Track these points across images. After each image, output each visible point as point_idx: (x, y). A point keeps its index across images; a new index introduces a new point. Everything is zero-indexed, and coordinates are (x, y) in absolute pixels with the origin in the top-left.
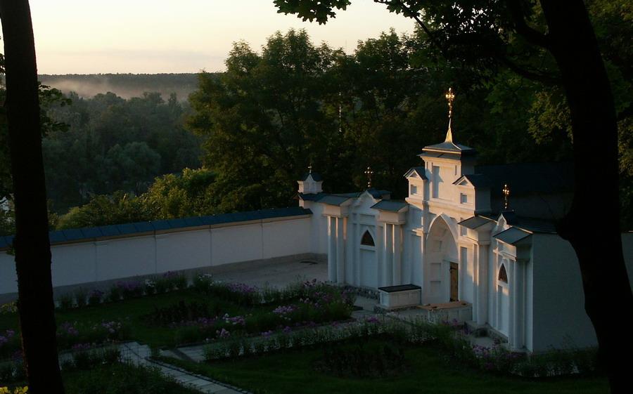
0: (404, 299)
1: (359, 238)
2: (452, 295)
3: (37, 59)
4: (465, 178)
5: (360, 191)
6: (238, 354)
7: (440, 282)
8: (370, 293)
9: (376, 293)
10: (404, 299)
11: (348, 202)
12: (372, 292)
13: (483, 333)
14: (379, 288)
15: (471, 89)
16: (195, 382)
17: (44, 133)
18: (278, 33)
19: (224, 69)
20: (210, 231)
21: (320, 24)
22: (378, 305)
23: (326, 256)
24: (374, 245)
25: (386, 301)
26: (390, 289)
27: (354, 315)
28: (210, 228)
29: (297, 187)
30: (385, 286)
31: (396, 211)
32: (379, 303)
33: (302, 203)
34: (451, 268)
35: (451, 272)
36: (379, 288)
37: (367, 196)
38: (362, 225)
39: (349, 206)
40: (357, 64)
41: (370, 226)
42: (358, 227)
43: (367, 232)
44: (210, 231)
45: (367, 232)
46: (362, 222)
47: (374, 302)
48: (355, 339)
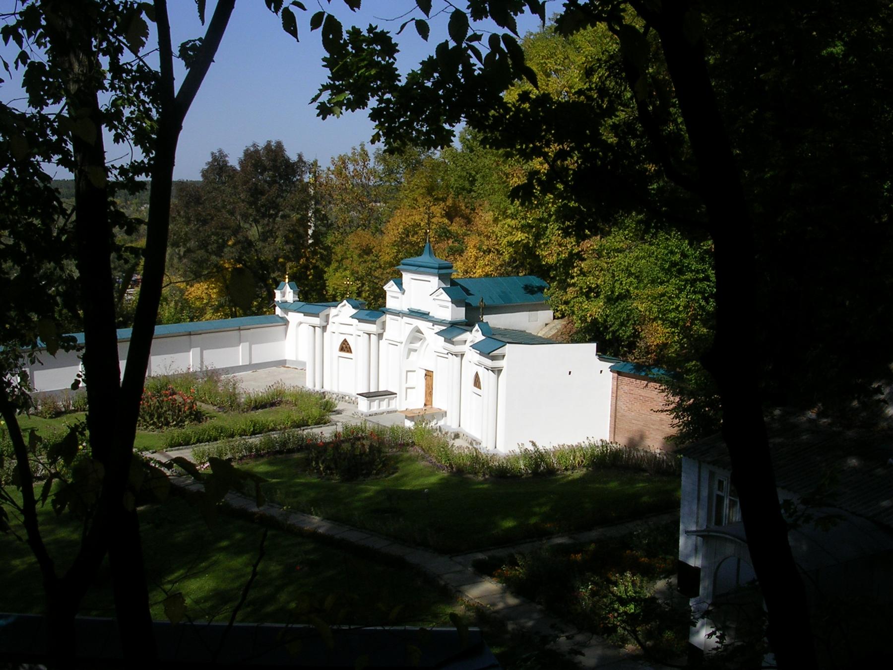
2: (426, 400)
3: (188, 112)
4: (441, 290)
8: (347, 398)
12: (349, 398)
13: (457, 436)
15: (397, 83)
18: (254, 145)
19: (198, 178)
21: (398, 51)
23: (304, 364)
25: (363, 405)
26: (369, 395)
27: (334, 417)
29: (274, 295)
33: (278, 311)
34: (426, 375)
35: (426, 379)
37: (345, 305)
43: (345, 341)
45: (345, 341)
47: (351, 407)
48: (337, 442)
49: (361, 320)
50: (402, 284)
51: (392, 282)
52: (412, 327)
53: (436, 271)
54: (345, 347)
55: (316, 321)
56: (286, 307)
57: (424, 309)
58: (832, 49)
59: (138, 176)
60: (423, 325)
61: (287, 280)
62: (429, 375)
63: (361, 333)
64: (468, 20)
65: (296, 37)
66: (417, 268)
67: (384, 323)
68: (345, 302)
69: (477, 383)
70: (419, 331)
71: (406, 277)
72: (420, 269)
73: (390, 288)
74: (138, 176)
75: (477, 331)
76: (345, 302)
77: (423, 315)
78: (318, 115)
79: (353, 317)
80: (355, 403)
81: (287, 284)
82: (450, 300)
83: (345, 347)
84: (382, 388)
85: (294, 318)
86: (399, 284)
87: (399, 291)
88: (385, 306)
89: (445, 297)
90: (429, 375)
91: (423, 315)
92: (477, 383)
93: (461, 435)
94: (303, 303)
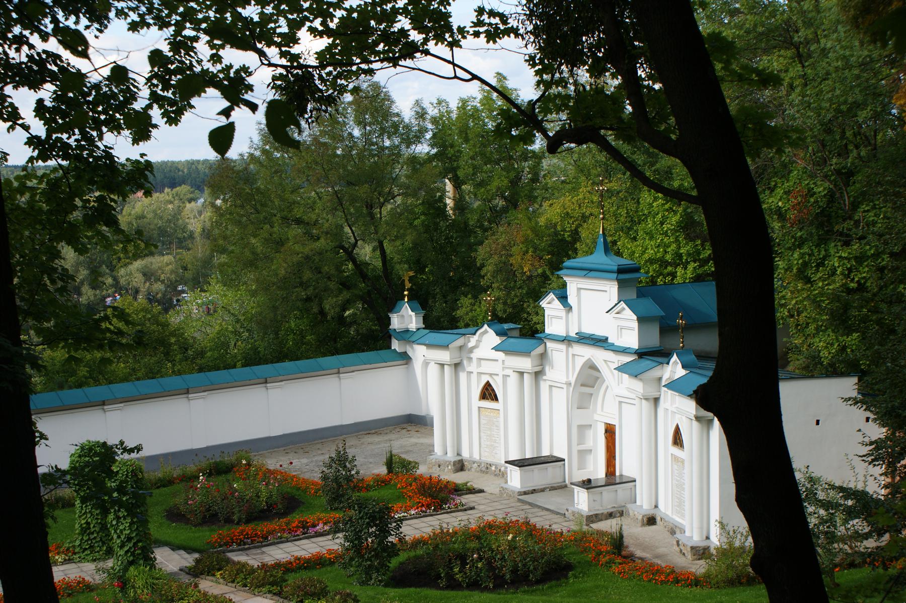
0: (540, 476)
1: (477, 391)
4: (623, 305)
5: (474, 324)
6: (891, 536)
7: (591, 450)
9: (503, 469)
10: (540, 476)
11: (460, 341)
12: (496, 468)
14: (506, 462)
16: (232, 596)
17: (271, 143)
20: (339, 377)
22: (505, 486)
24: (496, 399)
26: (521, 463)
28: (339, 373)
30: (510, 459)
31: (526, 353)
32: (506, 482)
33: (396, 345)
36: (506, 462)
37: (486, 332)
38: (480, 374)
39: (461, 348)
40: (574, 103)
41: (491, 375)
42: (474, 377)
44: (339, 377)
46: (481, 370)
47: (499, 482)
49: (508, 352)
50: (566, 297)
51: (551, 296)
52: (583, 360)
53: (615, 275)
54: (488, 393)
55: (444, 356)
56: (406, 335)
57: (599, 332)
58: (448, 208)
59: (436, 44)
60: (598, 355)
61: (406, 300)
62: (610, 432)
63: (509, 372)
64: (303, 26)
65: (89, 59)
66: (587, 272)
67: (543, 356)
68: (486, 326)
69: (677, 440)
70: (593, 367)
71: (573, 285)
72: (589, 272)
73: (550, 305)
74: (436, 44)
75: (675, 362)
76: (486, 326)
77: (600, 342)
78: (472, 22)
79: (496, 348)
80: (503, 475)
81: (406, 304)
82: (635, 317)
83: (488, 393)
84: (545, 452)
85: (419, 353)
86: (563, 298)
87: (562, 307)
88: (544, 331)
89: (629, 314)
90: (610, 432)
91: (600, 342)
92: (677, 440)
93: (658, 519)
94: (427, 331)
